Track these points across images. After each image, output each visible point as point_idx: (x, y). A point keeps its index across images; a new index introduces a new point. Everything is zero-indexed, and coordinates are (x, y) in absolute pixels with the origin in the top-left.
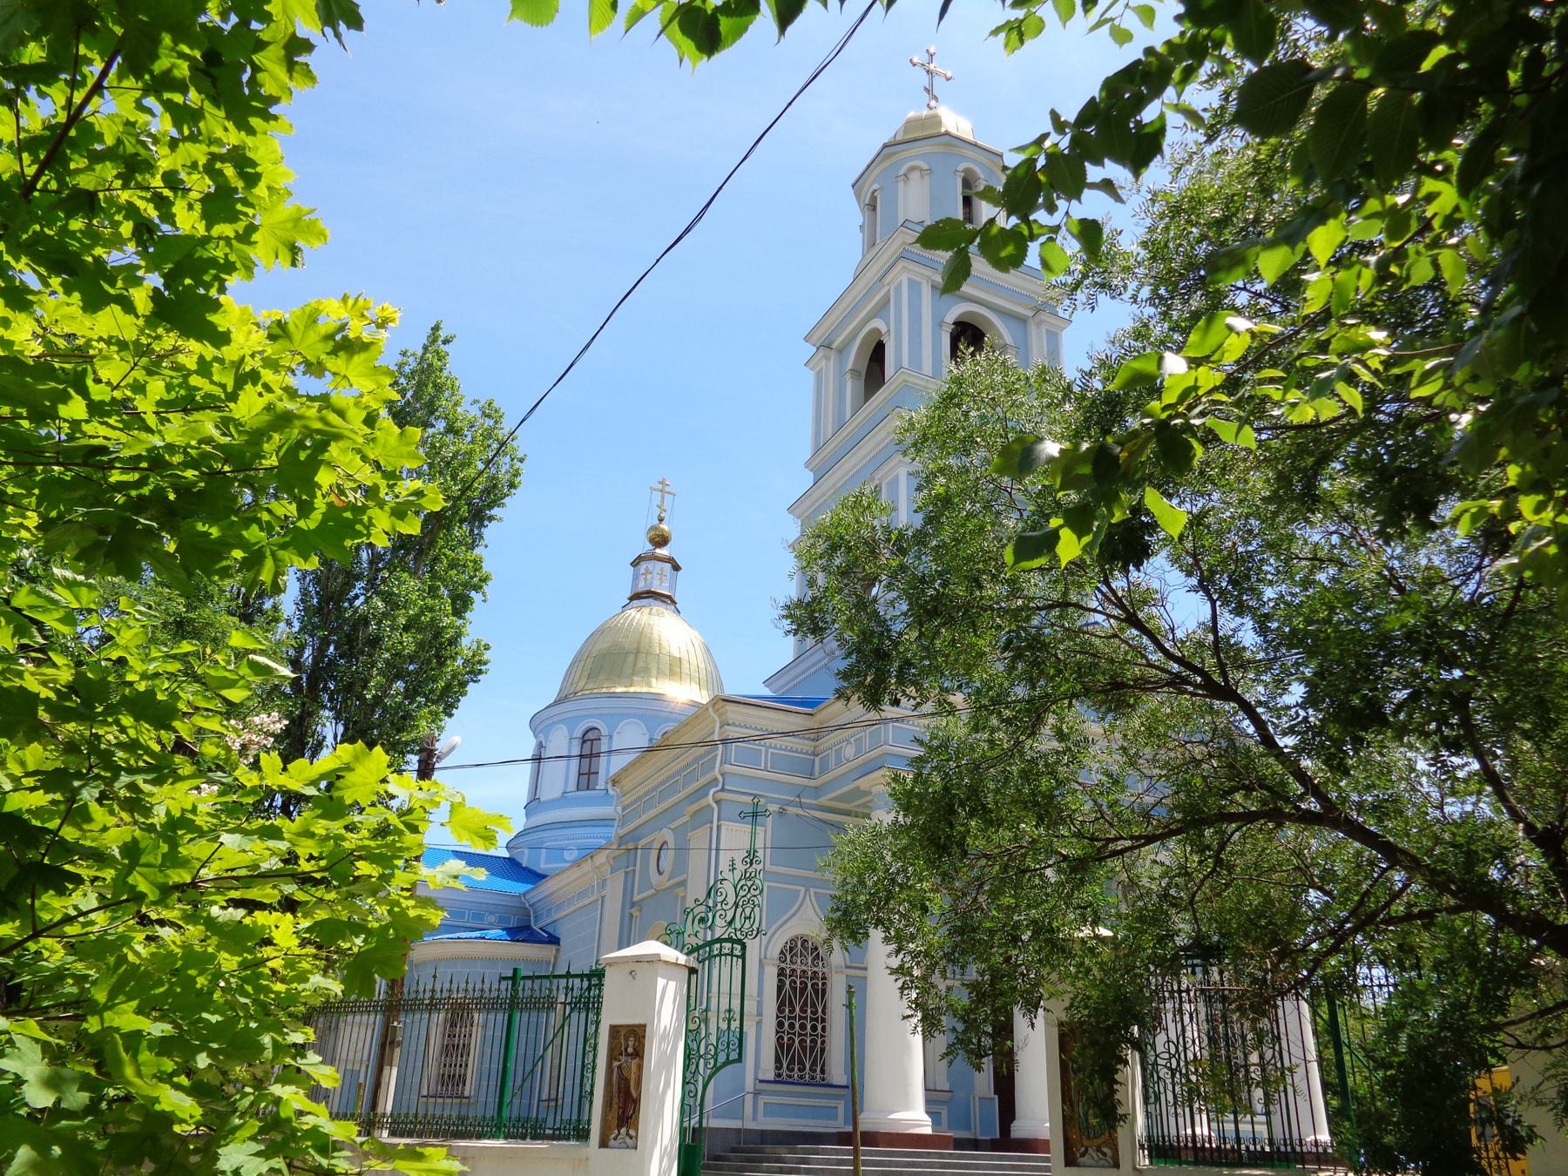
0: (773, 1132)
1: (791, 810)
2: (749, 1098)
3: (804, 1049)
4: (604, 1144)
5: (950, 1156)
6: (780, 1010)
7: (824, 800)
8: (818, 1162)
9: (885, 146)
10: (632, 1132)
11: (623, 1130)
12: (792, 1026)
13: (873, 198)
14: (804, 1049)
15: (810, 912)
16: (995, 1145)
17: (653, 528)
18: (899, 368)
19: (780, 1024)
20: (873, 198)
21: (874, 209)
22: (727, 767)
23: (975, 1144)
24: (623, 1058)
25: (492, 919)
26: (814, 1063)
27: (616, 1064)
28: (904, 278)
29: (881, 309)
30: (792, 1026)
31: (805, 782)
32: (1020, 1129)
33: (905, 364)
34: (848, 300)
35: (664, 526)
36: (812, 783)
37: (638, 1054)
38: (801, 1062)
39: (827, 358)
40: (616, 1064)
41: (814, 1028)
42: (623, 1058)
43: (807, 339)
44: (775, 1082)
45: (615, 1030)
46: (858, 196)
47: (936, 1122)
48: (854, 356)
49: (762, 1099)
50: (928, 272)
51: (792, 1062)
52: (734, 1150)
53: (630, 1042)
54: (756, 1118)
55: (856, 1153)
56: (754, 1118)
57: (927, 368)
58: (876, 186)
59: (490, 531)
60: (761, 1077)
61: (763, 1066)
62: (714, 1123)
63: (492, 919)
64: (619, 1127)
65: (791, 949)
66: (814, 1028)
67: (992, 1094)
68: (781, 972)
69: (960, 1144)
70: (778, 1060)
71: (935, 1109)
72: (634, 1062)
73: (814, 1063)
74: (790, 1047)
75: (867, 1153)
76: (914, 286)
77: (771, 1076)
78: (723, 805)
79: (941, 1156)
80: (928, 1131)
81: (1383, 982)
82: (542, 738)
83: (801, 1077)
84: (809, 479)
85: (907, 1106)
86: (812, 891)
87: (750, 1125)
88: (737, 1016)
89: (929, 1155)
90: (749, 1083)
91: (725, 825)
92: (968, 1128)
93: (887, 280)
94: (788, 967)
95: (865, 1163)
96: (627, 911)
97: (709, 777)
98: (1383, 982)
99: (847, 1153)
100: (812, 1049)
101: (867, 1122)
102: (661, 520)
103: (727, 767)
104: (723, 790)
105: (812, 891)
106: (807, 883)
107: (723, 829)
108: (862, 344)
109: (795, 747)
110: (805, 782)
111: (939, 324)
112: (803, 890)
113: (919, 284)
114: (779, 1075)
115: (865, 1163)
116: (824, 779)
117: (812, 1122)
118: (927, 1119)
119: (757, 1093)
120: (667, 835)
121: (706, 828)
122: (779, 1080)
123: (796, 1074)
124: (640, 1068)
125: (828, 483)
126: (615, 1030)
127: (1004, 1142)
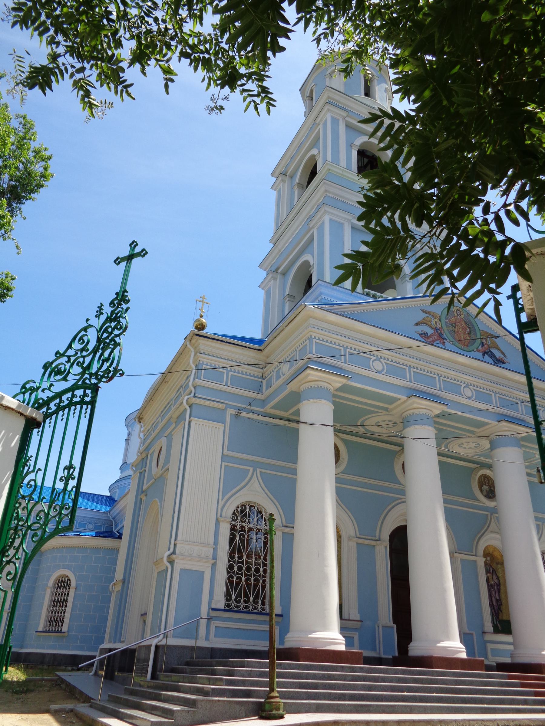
0: (221, 649)
2: (203, 622)
3: (248, 585)
5: (361, 670)
6: (231, 556)
7: (268, 409)
8: (242, 674)
12: (240, 568)
14: (248, 585)
15: (256, 485)
16: (395, 662)
17: (198, 320)
18: (325, 161)
19: (231, 567)
20: (312, 91)
21: (312, 99)
22: (198, 381)
23: (379, 661)
25: (91, 526)
26: (257, 597)
28: (329, 116)
29: (315, 143)
30: (240, 568)
31: (254, 395)
32: (417, 648)
33: (329, 158)
34: (296, 142)
35: (204, 320)
36: (260, 397)
38: (246, 596)
39: (284, 181)
41: (257, 570)
43: (272, 175)
44: (224, 610)
47: (349, 642)
49: (214, 624)
50: (349, 217)
51: (239, 596)
52: (188, 664)
54: (207, 639)
55: (271, 666)
56: (207, 638)
57: (343, 162)
59: (27, 207)
60: (214, 606)
61: (215, 598)
62: (172, 642)
63: (91, 526)
65: (242, 512)
66: (257, 570)
67: (391, 623)
68: (233, 528)
69: (368, 661)
70: (228, 594)
71: (350, 634)
73: (257, 597)
74: (238, 584)
75: (284, 667)
76: (335, 121)
77: (222, 605)
78: (194, 407)
79: (353, 670)
80: (342, 648)
82: (130, 430)
83: (246, 607)
85: (325, 627)
86: (258, 470)
87: (202, 643)
88: (76, 474)
89: (343, 669)
90: (204, 611)
91: (194, 421)
92: (374, 649)
94: (238, 524)
95: (280, 675)
96: (139, 497)
99: (262, 665)
100: (255, 586)
101: (292, 640)
102: (201, 317)
103: (198, 381)
104: (194, 396)
105: (258, 470)
106: (255, 465)
108: (304, 167)
109: (249, 372)
110: (254, 395)
111: (350, 145)
112: (251, 469)
113: (338, 120)
114: (228, 606)
115: (280, 675)
116: (270, 391)
117: (252, 642)
118: (342, 640)
119: (210, 619)
122: (228, 609)
123: (242, 605)
125: (281, 244)
127: (403, 658)
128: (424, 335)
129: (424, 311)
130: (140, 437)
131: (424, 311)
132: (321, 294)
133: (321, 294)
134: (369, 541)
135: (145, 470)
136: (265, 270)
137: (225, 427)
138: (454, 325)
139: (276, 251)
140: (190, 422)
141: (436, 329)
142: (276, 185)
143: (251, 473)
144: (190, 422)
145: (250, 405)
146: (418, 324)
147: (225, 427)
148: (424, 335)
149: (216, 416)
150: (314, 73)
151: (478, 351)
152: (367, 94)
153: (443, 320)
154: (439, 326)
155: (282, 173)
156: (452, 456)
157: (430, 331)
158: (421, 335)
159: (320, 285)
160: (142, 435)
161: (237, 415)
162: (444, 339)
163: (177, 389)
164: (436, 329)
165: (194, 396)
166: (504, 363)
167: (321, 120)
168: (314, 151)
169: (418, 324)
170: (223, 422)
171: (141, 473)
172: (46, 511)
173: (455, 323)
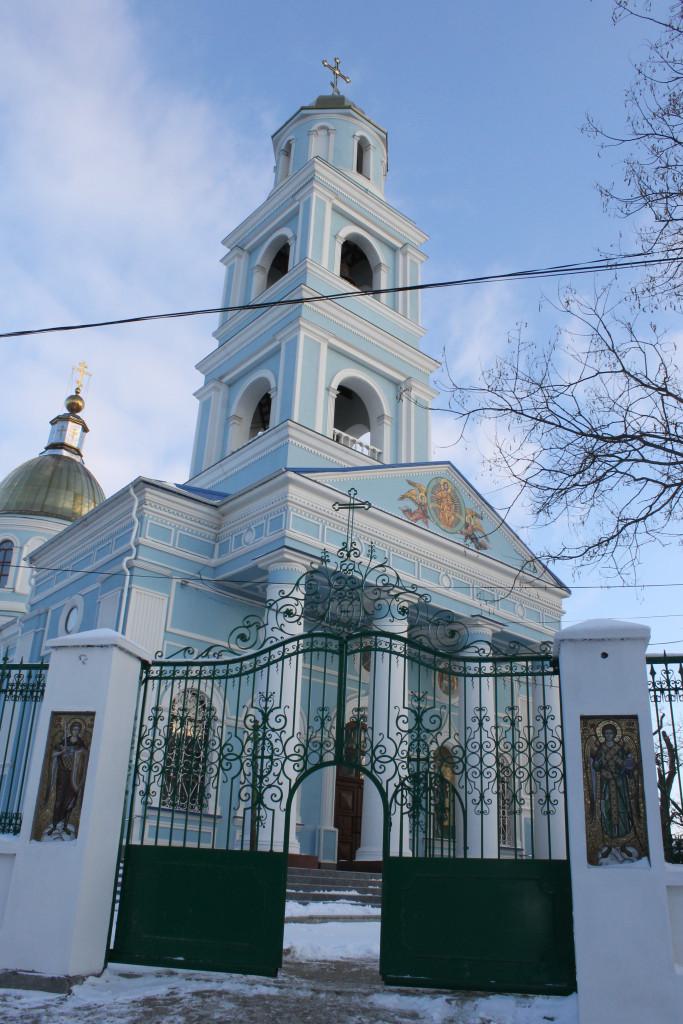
1: (192, 584)
4: (37, 835)
9: (302, 108)
10: (70, 827)
11: (60, 825)
13: (289, 146)
22: (141, 540)
24: (65, 748)
27: (56, 753)
37: (84, 744)
40: (56, 753)
42: (65, 748)
45: (56, 716)
46: (275, 144)
48: (263, 258)
53: (73, 736)
58: (291, 137)
64: (55, 821)
72: (77, 754)
81: (665, 686)
84: (214, 344)
93: (298, 197)
97: (124, 548)
98: (665, 686)
107: (134, 591)
108: (270, 247)
120: (79, 600)
121: (120, 588)
124: (85, 759)
125: (231, 346)
126: (56, 716)
128: (407, 512)
129: (410, 483)
130: (30, 584)
131: (410, 483)
132: (288, 436)
133: (288, 436)
134: (155, 567)
135: (43, 631)
136: (203, 373)
137: (169, 598)
138: (439, 501)
139: (223, 353)
140: (130, 590)
141: (420, 505)
142: (228, 259)
143: (168, 626)
144: (130, 590)
145: (199, 573)
146: (403, 498)
147: (169, 598)
148: (407, 512)
149: (161, 579)
150: (295, 122)
151: (462, 533)
152: (360, 169)
153: (429, 495)
154: (424, 501)
155: (238, 244)
156: (355, 219)
157: (414, 508)
158: (404, 511)
159: (288, 426)
160: (33, 581)
161: (183, 585)
162: (428, 517)
163: (103, 538)
164: (420, 505)
165: (136, 558)
166: (485, 548)
167: (302, 197)
168: (286, 232)
169: (403, 498)
170: (169, 593)
171: (36, 633)
172: (221, 771)
173: (442, 498)
